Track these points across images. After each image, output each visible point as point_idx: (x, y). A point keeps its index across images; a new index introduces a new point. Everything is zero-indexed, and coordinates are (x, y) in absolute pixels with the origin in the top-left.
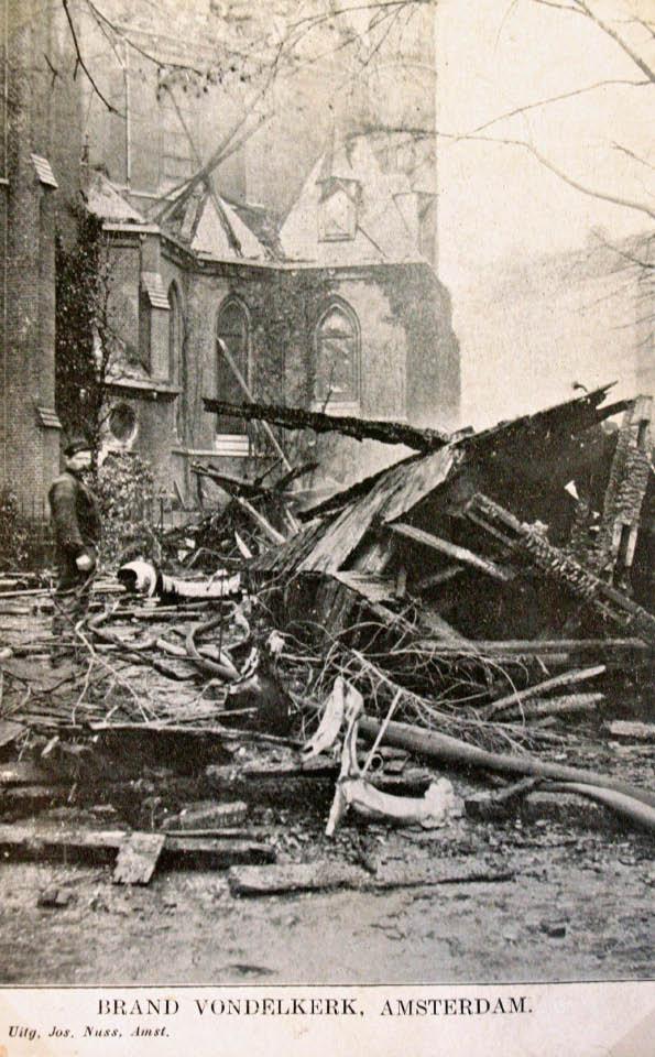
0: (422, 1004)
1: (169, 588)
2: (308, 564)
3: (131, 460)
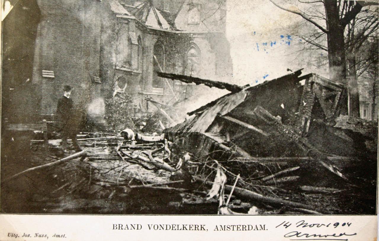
0: (229, 227)
1: (140, 138)
2: (193, 130)
3: (125, 95)
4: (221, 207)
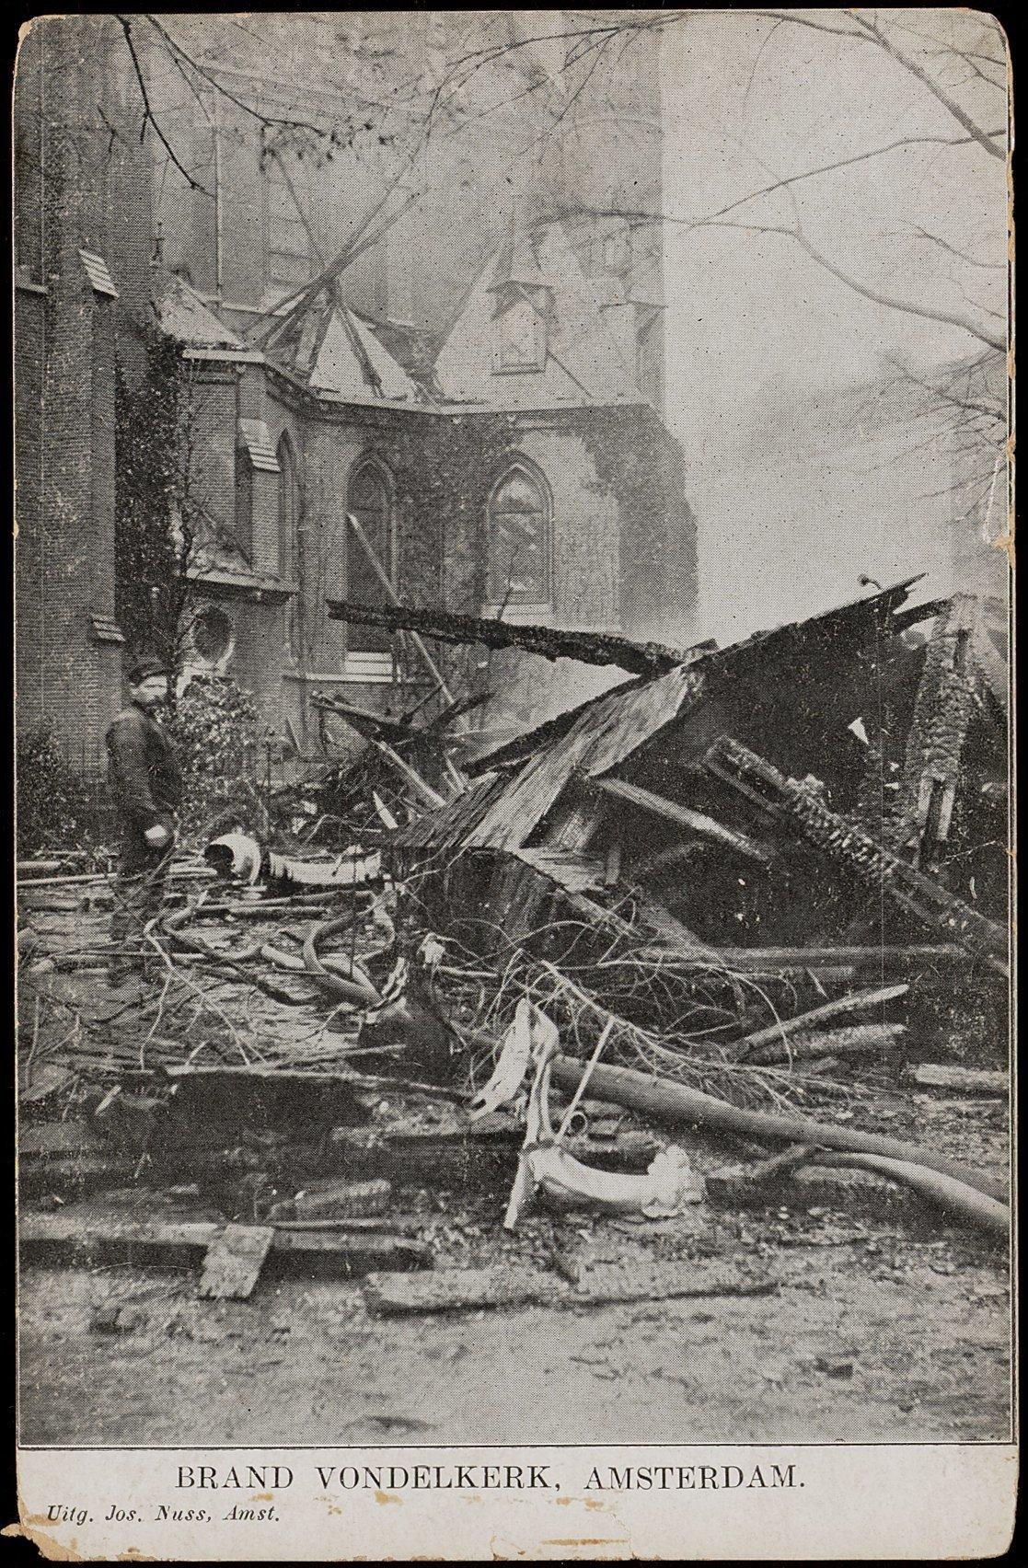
1: (279, 873)
2: (479, 835)
4: (532, 1147)
